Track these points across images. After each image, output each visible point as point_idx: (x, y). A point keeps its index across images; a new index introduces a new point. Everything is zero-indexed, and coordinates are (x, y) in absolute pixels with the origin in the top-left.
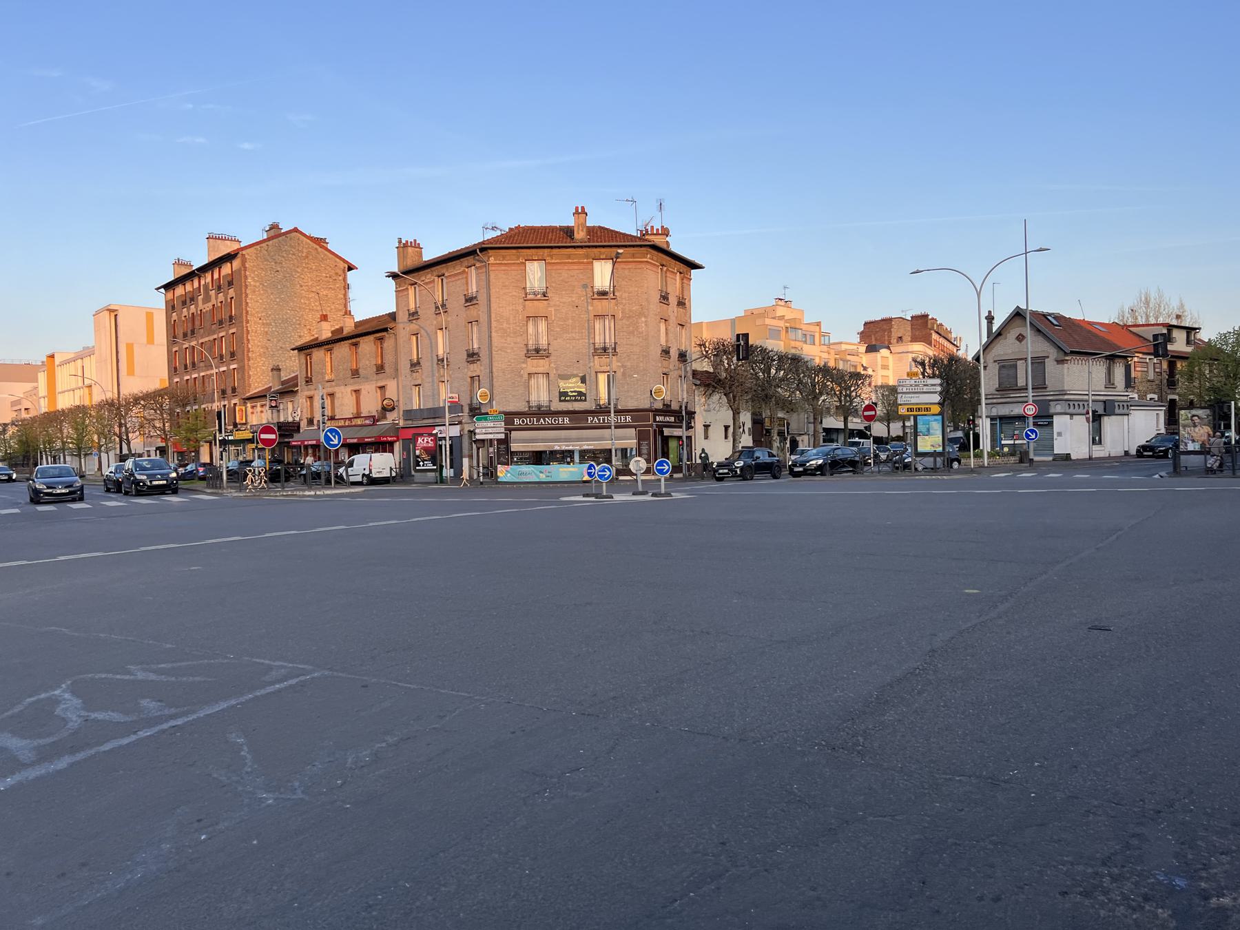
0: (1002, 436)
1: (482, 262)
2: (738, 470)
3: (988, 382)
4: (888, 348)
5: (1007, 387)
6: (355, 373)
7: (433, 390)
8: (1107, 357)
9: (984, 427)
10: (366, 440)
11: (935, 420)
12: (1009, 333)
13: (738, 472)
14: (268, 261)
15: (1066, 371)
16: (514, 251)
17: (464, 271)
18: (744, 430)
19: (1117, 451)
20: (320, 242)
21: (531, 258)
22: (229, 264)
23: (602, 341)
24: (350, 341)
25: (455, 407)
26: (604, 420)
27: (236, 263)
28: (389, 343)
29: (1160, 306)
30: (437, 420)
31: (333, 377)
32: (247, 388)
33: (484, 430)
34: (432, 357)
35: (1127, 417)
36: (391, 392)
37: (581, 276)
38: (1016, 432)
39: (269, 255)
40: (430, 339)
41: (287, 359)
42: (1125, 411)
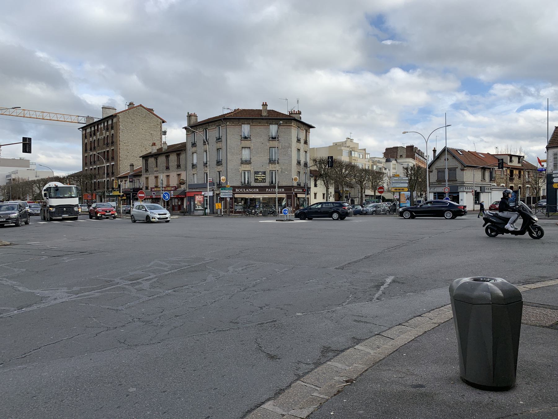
5: (440, 181)
12: (442, 157)
18: (331, 195)
20: (150, 110)
25: (212, 184)
26: (273, 190)
35: (490, 193)
36: (183, 177)
41: (135, 161)
42: (490, 191)
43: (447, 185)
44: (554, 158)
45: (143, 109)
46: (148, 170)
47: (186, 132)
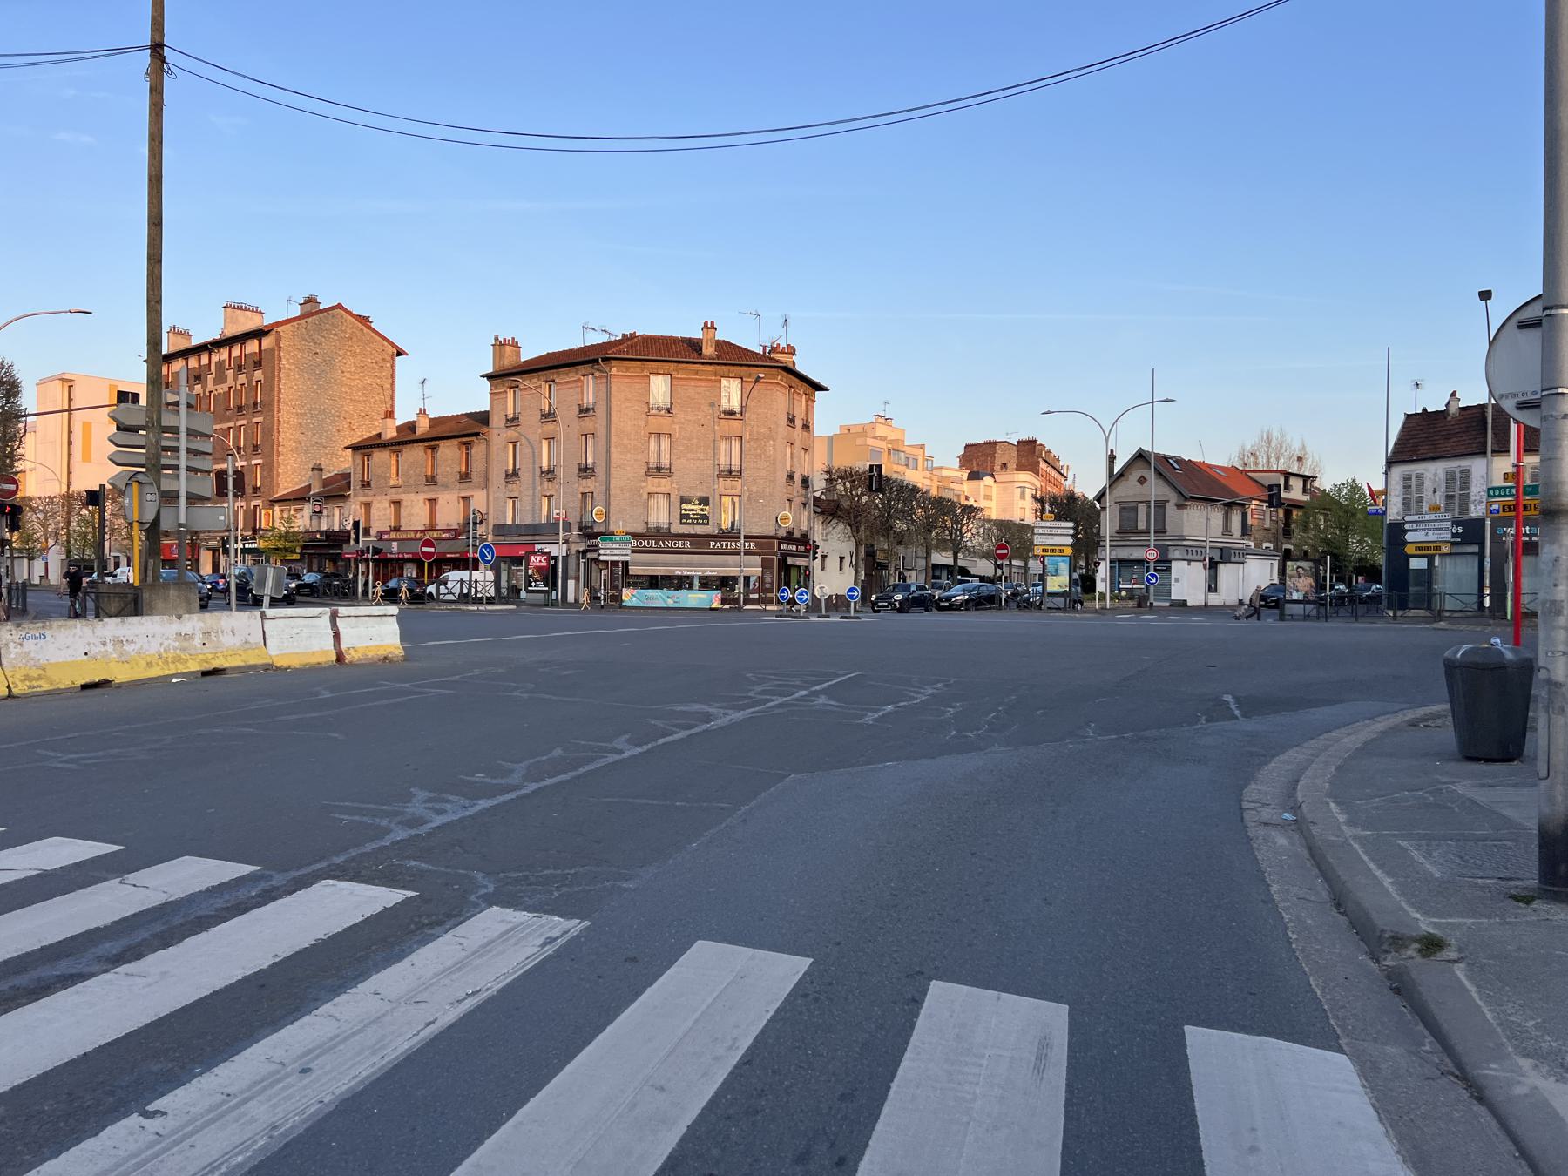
0: (1121, 579)
1: (601, 371)
2: (897, 603)
3: (1108, 524)
4: (993, 476)
5: (1127, 530)
6: (431, 480)
7: (534, 504)
8: (1224, 505)
9: (1103, 571)
10: (448, 555)
11: (1063, 561)
12: (1131, 474)
13: (898, 606)
14: (306, 340)
15: (1185, 516)
16: (639, 363)
17: (579, 379)
19: (1232, 599)
20: (364, 320)
21: (655, 371)
22: (256, 342)
23: (728, 463)
24: (426, 444)
26: (727, 545)
27: (267, 342)
28: (478, 450)
29: (1281, 447)
30: (537, 538)
31: (400, 482)
32: (275, 488)
33: (608, 551)
34: (534, 469)
35: (1241, 566)
37: (708, 394)
38: (1135, 576)
39: (307, 334)
40: (533, 448)
43: (1153, 543)
44: (1404, 487)
45: (346, 315)
46: (369, 484)
47: (491, 386)
